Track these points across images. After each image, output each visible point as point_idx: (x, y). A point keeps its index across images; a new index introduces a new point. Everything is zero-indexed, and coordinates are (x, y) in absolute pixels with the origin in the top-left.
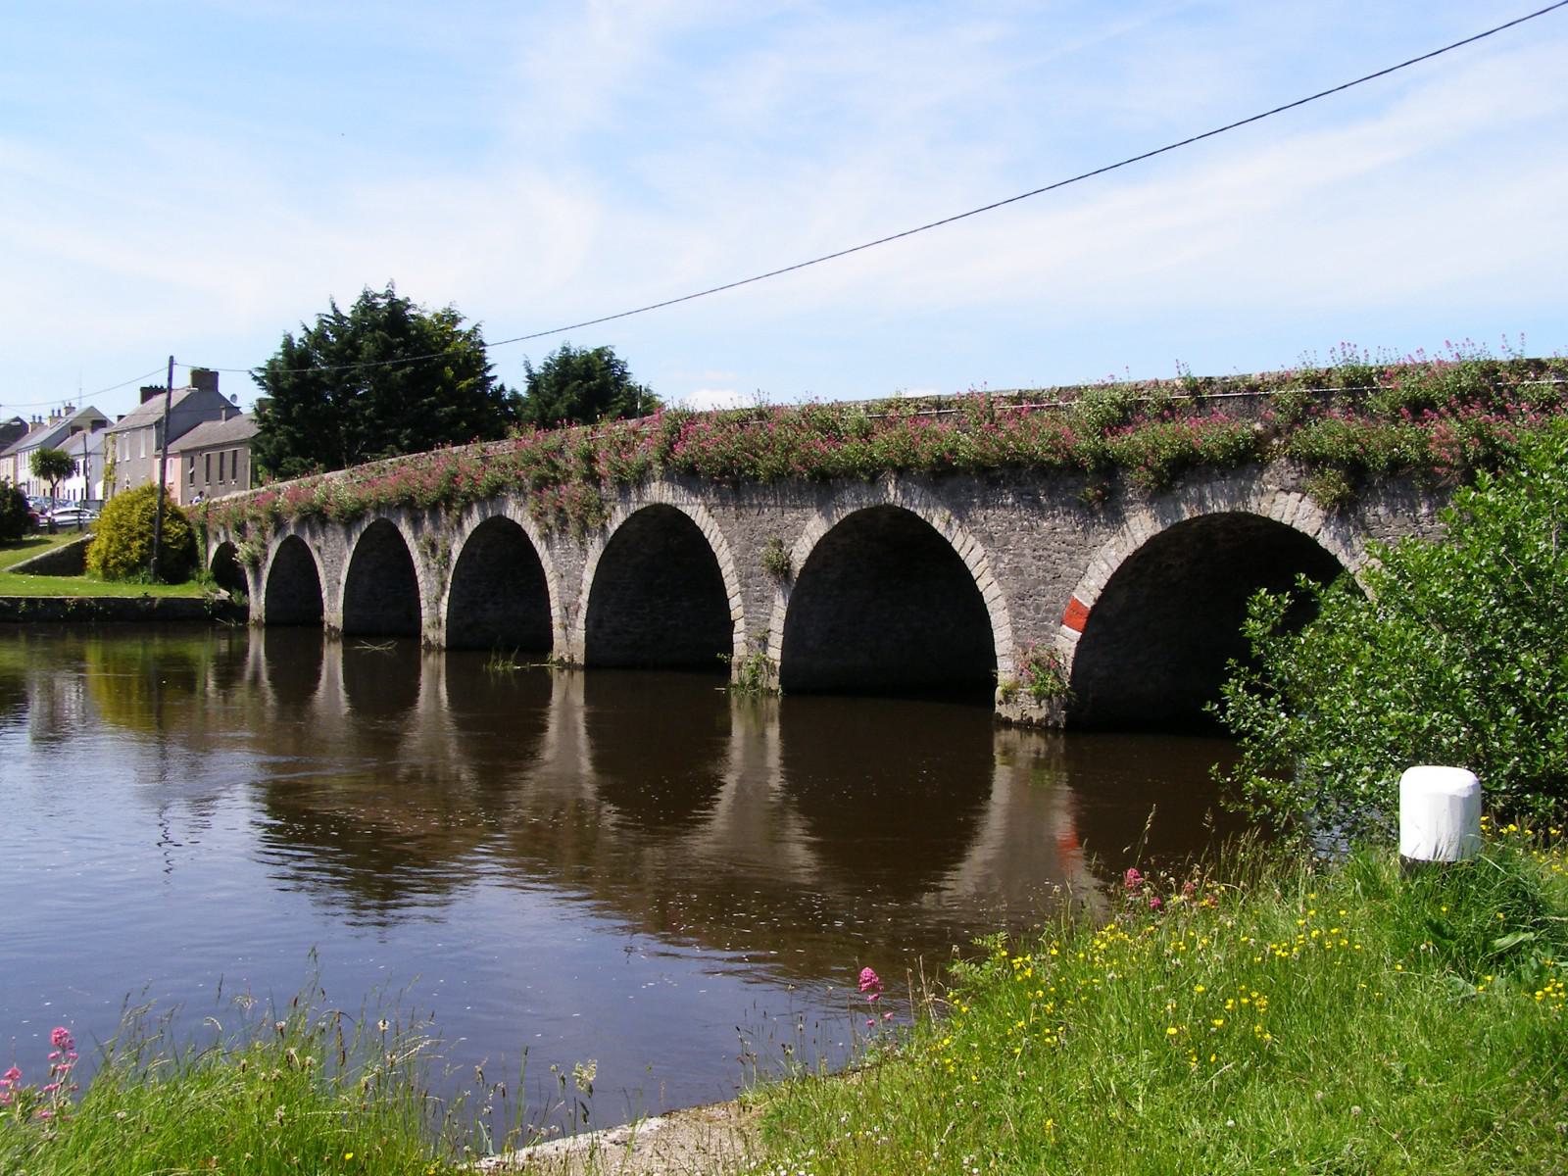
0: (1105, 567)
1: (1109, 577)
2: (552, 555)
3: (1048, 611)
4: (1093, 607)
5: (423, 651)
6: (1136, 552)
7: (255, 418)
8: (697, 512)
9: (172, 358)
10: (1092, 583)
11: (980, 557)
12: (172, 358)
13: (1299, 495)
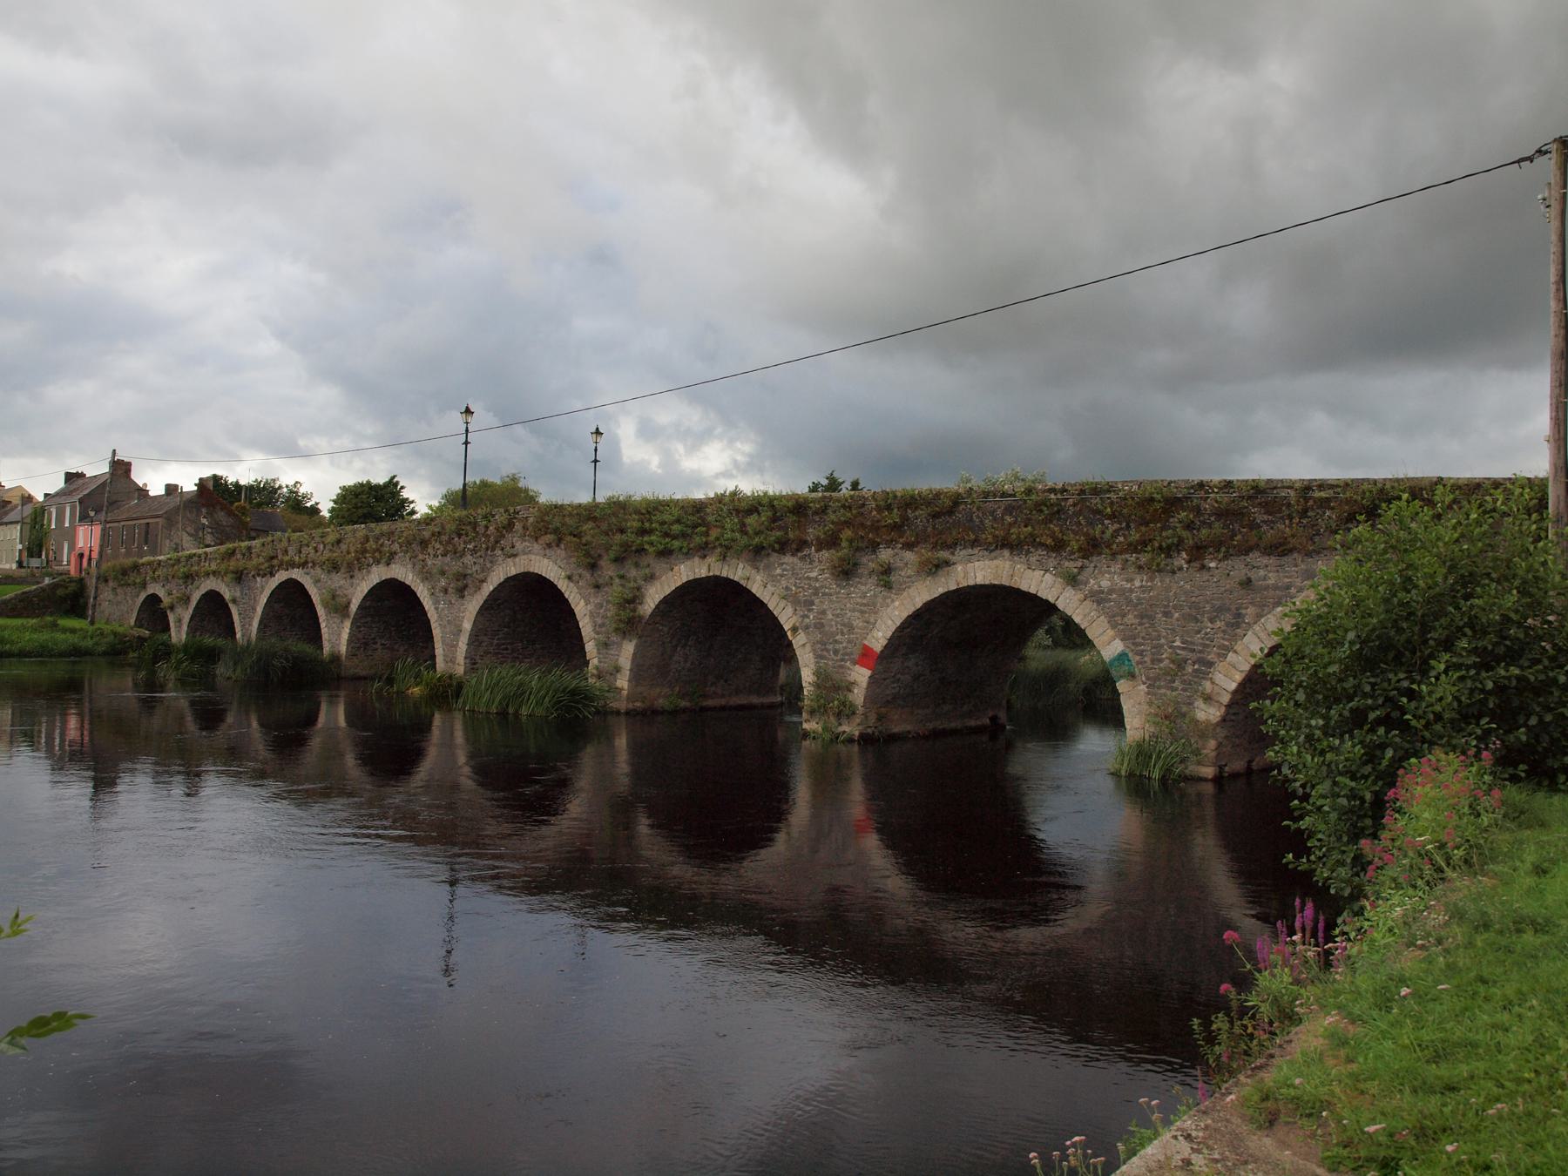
0: (890, 622)
2: (436, 609)
3: (847, 654)
4: (882, 651)
5: (789, 634)
8: (738, 571)
10: (880, 634)
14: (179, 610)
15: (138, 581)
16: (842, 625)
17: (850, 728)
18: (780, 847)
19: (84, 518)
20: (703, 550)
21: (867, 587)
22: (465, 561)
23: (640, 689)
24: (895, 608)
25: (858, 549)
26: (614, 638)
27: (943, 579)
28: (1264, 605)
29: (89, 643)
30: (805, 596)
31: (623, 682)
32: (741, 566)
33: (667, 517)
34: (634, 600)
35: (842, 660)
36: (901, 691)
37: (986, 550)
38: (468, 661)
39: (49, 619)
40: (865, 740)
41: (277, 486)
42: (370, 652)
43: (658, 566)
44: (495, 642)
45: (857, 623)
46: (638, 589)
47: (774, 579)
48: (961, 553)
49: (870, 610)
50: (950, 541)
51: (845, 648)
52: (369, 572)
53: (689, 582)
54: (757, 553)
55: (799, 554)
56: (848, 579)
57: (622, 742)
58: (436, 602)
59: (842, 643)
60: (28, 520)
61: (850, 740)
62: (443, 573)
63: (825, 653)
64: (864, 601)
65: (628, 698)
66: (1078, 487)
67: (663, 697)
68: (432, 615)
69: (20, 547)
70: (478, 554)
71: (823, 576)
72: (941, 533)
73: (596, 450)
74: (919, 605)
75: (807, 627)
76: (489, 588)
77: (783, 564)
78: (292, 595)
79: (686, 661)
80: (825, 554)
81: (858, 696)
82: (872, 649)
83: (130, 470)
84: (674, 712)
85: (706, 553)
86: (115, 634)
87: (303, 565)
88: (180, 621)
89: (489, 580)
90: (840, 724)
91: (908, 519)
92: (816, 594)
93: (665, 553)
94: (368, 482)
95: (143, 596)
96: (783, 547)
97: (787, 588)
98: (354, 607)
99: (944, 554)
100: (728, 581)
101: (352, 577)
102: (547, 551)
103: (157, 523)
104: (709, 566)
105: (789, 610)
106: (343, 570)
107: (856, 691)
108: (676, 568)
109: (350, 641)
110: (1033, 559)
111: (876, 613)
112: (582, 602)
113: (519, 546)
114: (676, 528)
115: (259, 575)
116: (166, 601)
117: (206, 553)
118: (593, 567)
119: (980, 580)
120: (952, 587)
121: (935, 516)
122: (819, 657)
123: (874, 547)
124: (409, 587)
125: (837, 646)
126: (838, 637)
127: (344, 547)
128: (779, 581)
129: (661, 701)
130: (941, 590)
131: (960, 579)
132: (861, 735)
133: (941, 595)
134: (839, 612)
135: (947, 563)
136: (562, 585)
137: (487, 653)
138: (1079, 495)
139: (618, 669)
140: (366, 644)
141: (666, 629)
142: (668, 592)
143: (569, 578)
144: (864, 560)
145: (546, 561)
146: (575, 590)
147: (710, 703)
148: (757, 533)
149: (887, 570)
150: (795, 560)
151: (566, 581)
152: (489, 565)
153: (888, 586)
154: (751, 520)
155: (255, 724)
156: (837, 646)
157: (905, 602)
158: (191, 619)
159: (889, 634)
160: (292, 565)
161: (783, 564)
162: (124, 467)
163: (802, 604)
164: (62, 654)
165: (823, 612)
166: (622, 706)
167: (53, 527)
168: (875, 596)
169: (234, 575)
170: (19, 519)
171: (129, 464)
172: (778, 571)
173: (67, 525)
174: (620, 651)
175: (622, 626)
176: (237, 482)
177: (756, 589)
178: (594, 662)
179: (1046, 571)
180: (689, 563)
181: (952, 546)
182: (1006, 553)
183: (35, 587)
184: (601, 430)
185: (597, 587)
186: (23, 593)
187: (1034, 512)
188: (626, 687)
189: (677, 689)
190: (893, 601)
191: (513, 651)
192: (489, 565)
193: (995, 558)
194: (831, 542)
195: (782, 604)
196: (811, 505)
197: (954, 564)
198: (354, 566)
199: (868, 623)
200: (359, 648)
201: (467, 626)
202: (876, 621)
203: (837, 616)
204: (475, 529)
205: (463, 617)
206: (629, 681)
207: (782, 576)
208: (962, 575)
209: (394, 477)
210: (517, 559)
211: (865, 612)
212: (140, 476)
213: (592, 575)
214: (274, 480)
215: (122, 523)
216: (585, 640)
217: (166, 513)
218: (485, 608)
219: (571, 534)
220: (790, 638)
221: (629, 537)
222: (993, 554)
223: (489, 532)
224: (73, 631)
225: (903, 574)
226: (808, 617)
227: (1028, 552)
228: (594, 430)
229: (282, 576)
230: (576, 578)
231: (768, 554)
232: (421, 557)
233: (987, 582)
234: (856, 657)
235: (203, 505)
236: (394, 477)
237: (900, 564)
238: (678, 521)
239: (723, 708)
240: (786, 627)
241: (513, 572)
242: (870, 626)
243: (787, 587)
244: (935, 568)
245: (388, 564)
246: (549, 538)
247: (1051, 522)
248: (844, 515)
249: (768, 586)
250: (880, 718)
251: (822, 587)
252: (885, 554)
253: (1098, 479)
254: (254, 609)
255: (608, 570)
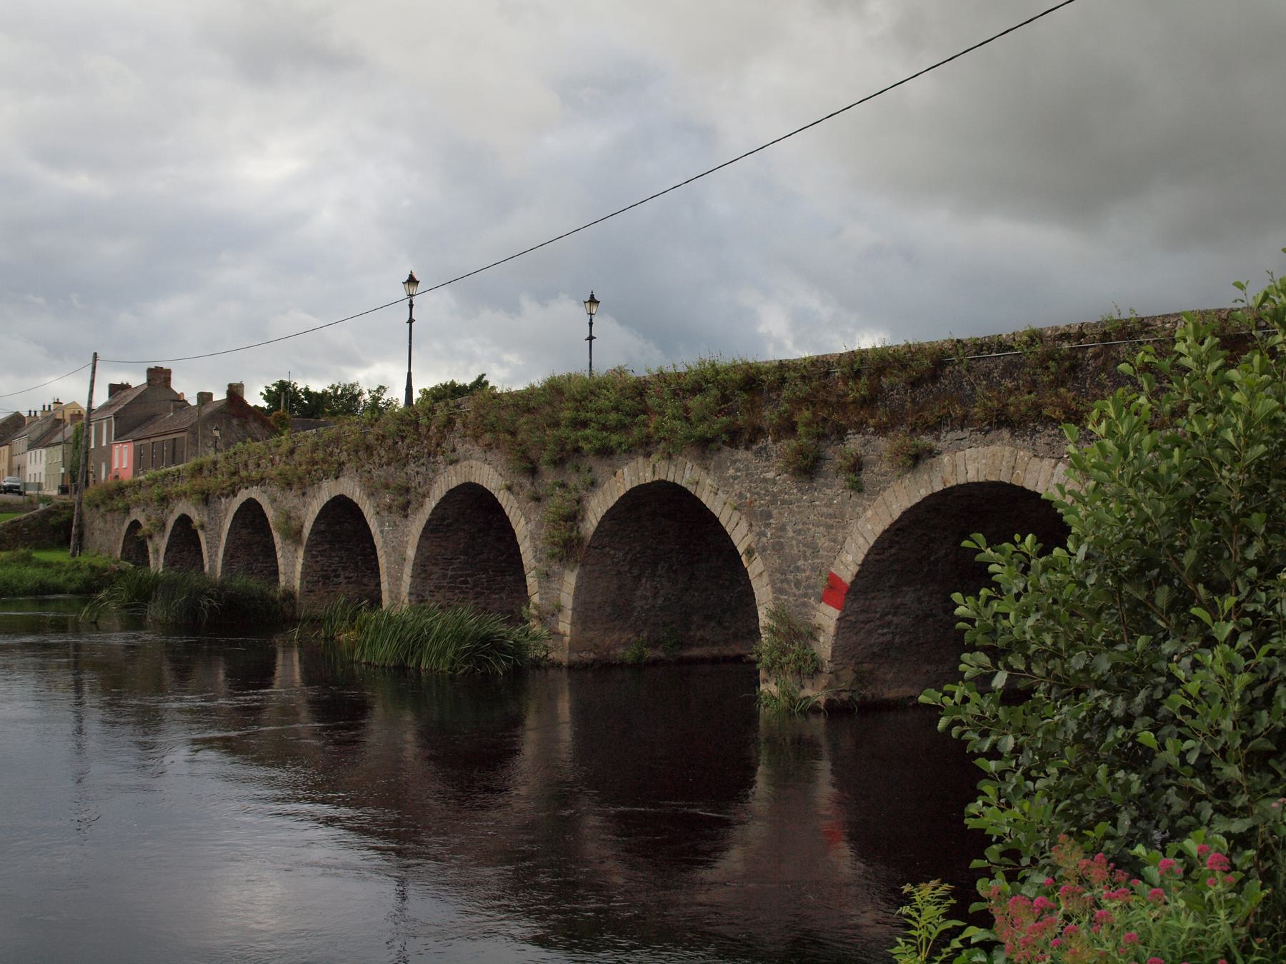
0: (861, 540)
1: (866, 551)
2: (382, 532)
3: (808, 587)
4: (853, 582)
5: (743, 558)
6: (892, 525)
7: (385, 397)
8: (686, 473)
9: (95, 354)
10: (850, 558)
11: (745, 533)
12: (95, 354)
13: (1053, 461)
14: (156, 539)
15: (120, 505)
16: (804, 545)
17: (816, 693)
18: (733, 860)
19: (120, 435)
20: (645, 446)
21: (832, 491)
22: (409, 472)
23: (589, 634)
24: (868, 520)
25: (821, 437)
26: (556, 568)
27: (926, 477)
28: (288, 464)
29: (61, 579)
30: (762, 505)
31: (565, 626)
32: (689, 465)
33: (603, 403)
34: (574, 517)
35: (806, 595)
36: (897, 640)
37: (980, 430)
38: (413, 598)
39: (22, 551)
40: (835, 710)
41: (356, 392)
42: (331, 588)
43: (601, 469)
44: (450, 573)
45: (823, 542)
46: (579, 501)
47: (725, 483)
48: (948, 437)
49: (838, 523)
50: (932, 420)
51: (808, 578)
52: (320, 488)
53: (632, 490)
54: (704, 447)
55: (754, 447)
56: (812, 479)
57: (564, 707)
58: (382, 524)
59: (804, 571)
60: (71, 441)
61: (815, 710)
62: (387, 486)
63: (785, 586)
64: (830, 511)
65: (572, 648)
66: (1100, 330)
67: (623, 645)
68: (378, 540)
69: (63, 470)
70: (422, 461)
71: (782, 477)
72: (922, 409)
73: (591, 324)
74: (896, 515)
75: (764, 549)
76: (431, 504)
77: (736, 461)
78: (251, 515)
79: (655, 596)
80: (784, 443)
81: (824, 646)
82: (840, 580)
83: (170, 379)
84: (639, 666)
85: (649, 449)
86: (93, 568)
87: (261, 481)
88: (157, 551)
89: (431, 494)
90: (802, 687)
91: (881, 390)
92: (773, 502)
93: (605, 452)
94: (453, 383)
95: (127, 523)
96: (735, 437)
97: (741, 495)
98: (306, 532)
99: (926, 440)
100: (674, 486)
101: (304, 494)
102: (489, 454)
103: (183, 438)
104: (654, 466)
105: (744, 526)
106: (295, 487)
107: (821, 639)
108: (620, 472)
109: (305, 574)
110: (1041, 441)
111: (844, 528)
112: (523, 519)
113: (461, 449)
114: (613, 416)
115: (222, 495)
116: (146, 527)
117: (178, 470)
118: (533, 471)
119: (972, 477)
120: (938, 487)
121: (914, 384)
122: (779, 591)
123: (841, 433)
124: (356, 505)
125: (800, 576)
126: (800, 563)
127: (296, 457)
128: (732, 485)
129: (621, 650)
130: (924, 493)
131: (947, 475)
132: (830, 702)
133: (924, 499)
134: (800, 527)
135: (931, 453)
136: (503, 498)
137: (438, 588)
138: (1101, 341)
139: (559, 609)
140: (326, 577)
141: (620, 554)
142: (611, 504)
143: (509, 488)
144: (829, 452)
145: (487, 467)
146: (516, 505)
147: (696, 652)
148: (703, 419)
149: (857, 466)
150: (749, 455)
151: (507, 493)
152: (431, 475)
153: (858, 488)
154: (695, 402)
155: (222, 677)
156: (800, 576)
157: (880, 511)
158: (168, 550)
159: (861, 558)
160: (251, 482)
161: (736, 461)
162: (162, 376)
163: (757, 516)
164: (27, 592)
165: (783, 528)
166: (561, 655)
167: (93, 447)
168: (843, 503)
169: (200, 496)
170: (61, 440)
171: (169, 372)
172: (731, 471)
173: (104, 444)
174: (562, 585)
175: (557, 550)
176: (307, 389)
177: (706, 498)
178: (535, 599)
179: (1060, 459)
180: (632, 464)
181: (934, 428)
182: (1006, 433)
183: (25, 515)
184: (596, 298)
185: (537, 499)
186: (12, 522)
187: (1039, 371)
188: (568, 632)
189: (645, 634)
190: (865, 510)
191: (475, 586)
192: (431, 475)
193: (992, 442)
194: (787, 428)
195: (737, 515)
196: (763, 377)
197: (940, 453)
198: (300, 483)
199: (834, 541)
200: (318, 581)
201: (411, 553)
202: (845, 538)
203: (799, 532)
204: (416, 429)
205: (407, 542)
206: (573, 624)
207: (735, 478)
208: (949, 469)
209: (483, 375)
210: (458, 467)
211: (831, 527)
212: (178, 385)
213: (532, 484)
214: (353, 386)
215: (152, 440)
216: (526, 570)
217: (191, 426)
218: (430, 529)
219: (977, 458)
220: (746, 565)
221: (563, 432)
222: (989, 437)
223: (431, 433)
224: (47, 565)
225: (876, 470)
226: (765, 535)
227: (1035, 431)
228: (588, 299)
229: (243, 496)
230: (516, 489)
231: (719, 449)
232: (367, 467)
233: (982, 479)
234: (820, 590)
235: (234, 416)
236: (483, 375)
237: (872, 456)
238: (616, 409)
239: (715, 660)
240: (741, 550)
241: (455, 482)
242: (838, 547)
243: (741, 494)
244: (917, 459)
245: (337, 478)
246: (488, 437)
247: (1063, 384)
248: (803, 390)
249: (720, 492)
250: (861, 679)
251: (781, 491)
252: (854, 443)
253: (1125, 315)
254: (220, 536)
255: (549, 476)
